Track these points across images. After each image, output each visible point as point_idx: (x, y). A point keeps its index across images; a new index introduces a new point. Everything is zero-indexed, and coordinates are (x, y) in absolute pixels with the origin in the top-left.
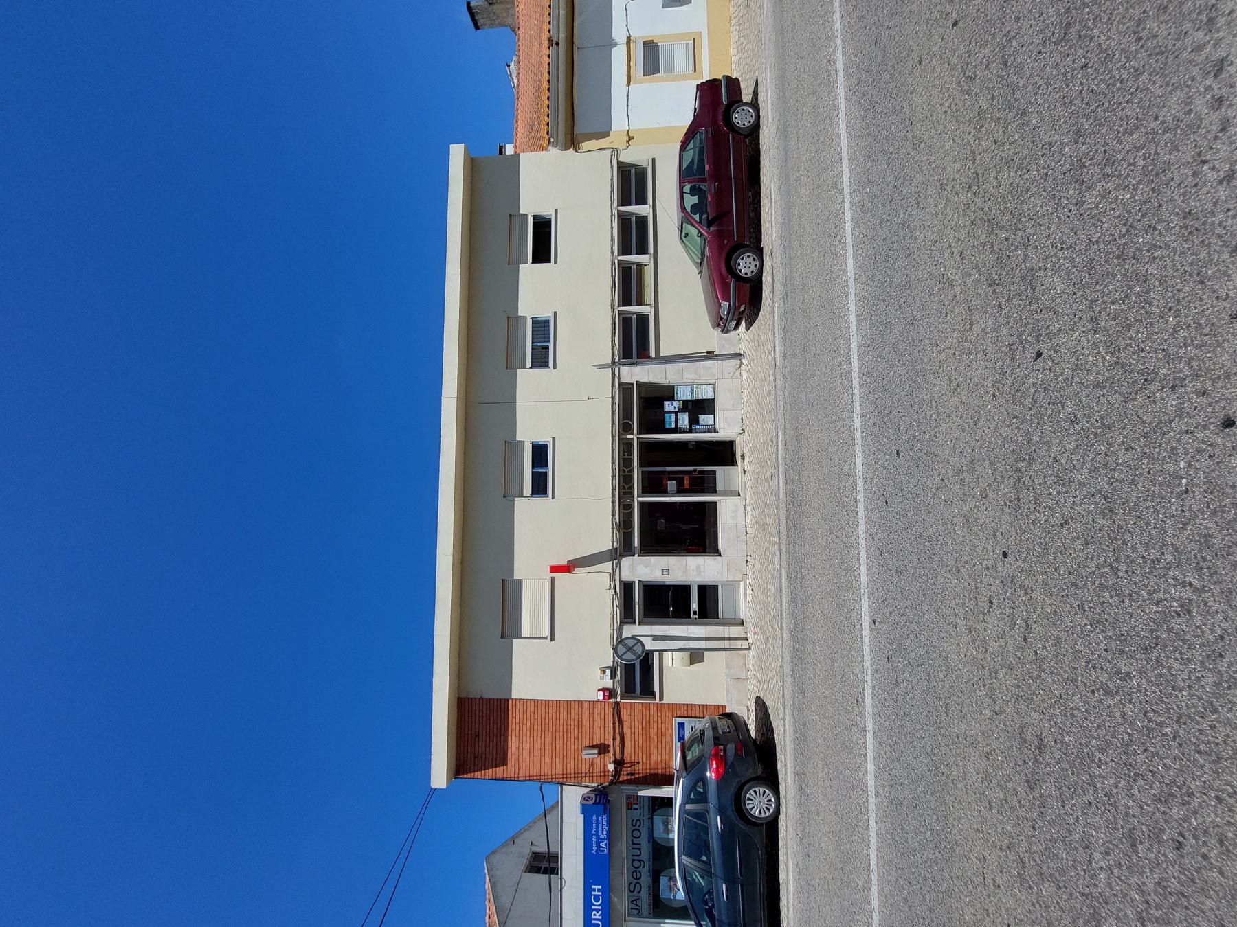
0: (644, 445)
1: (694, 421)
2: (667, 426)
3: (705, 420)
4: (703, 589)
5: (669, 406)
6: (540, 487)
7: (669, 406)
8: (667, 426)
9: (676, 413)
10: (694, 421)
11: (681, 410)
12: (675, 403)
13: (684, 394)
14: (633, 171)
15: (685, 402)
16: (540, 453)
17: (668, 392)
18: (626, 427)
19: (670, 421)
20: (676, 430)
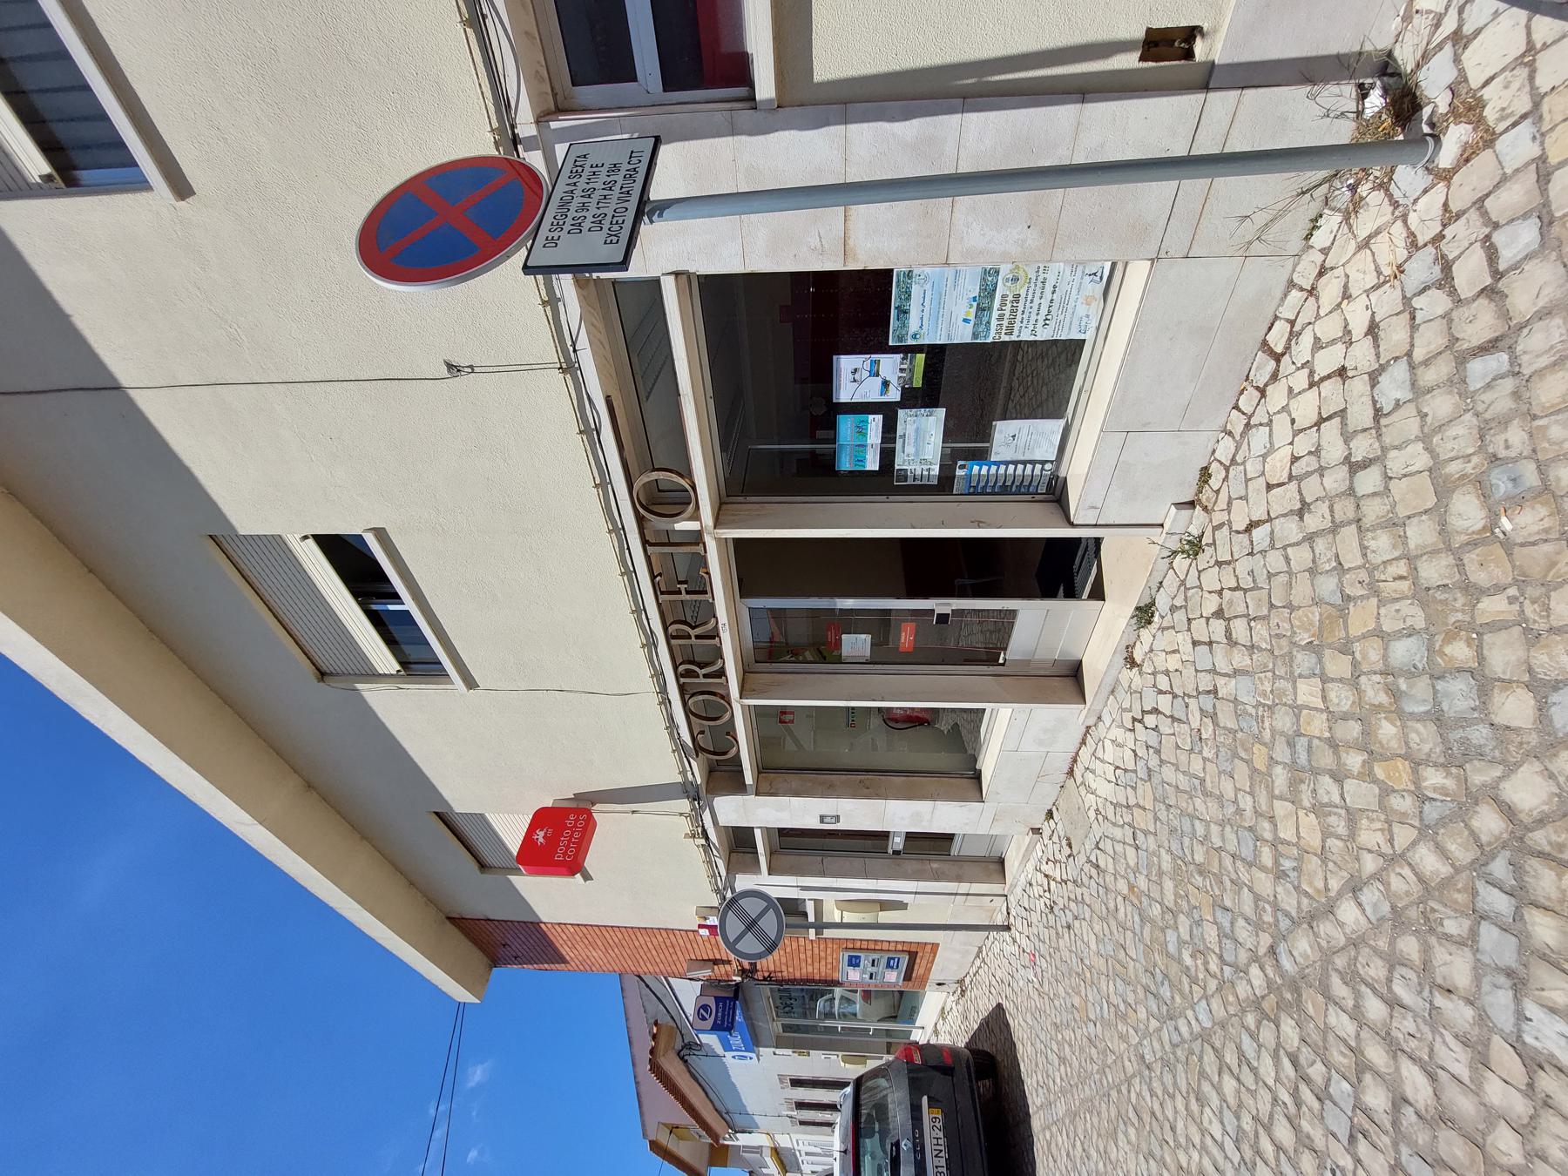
0: (758, 566)
1: (968, 435)
2: (845, 464)
3: (1018, 441)
4: (619, 67)
5: (858, 378)
6: (417, 661)
7: (858, 378)
8: (845, 464)
9: (889, 412)
10: (968, 435)
11: (915, 398)
12: (890, 364)
13: (936, 315)
14: (758, 833)
15: (936, 354)
16: (346, 554)
17: (852, 307)
18: (659, 501)
19: (860, 444)
20: (885, 481)
